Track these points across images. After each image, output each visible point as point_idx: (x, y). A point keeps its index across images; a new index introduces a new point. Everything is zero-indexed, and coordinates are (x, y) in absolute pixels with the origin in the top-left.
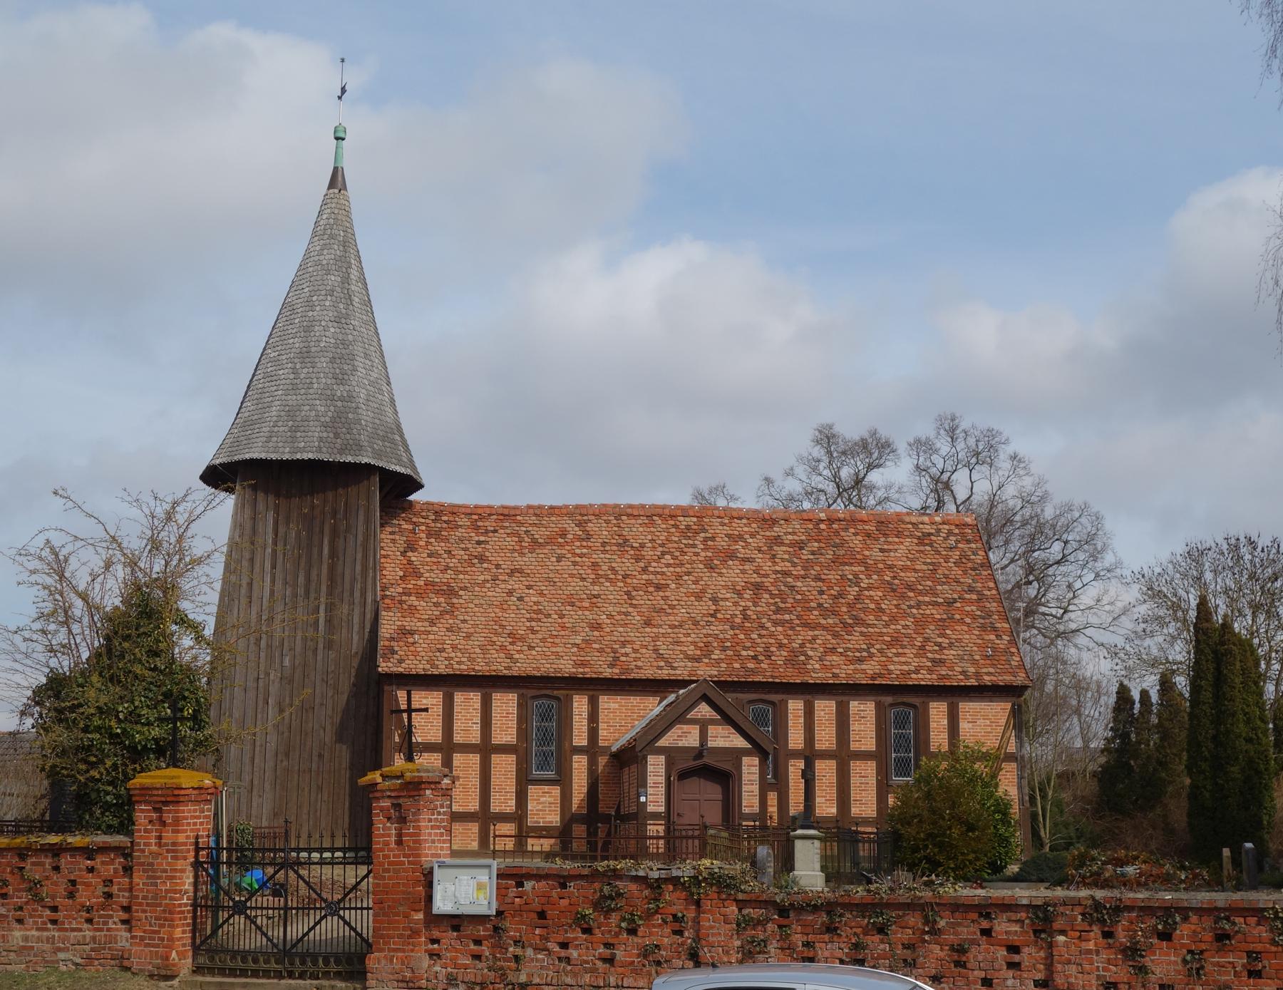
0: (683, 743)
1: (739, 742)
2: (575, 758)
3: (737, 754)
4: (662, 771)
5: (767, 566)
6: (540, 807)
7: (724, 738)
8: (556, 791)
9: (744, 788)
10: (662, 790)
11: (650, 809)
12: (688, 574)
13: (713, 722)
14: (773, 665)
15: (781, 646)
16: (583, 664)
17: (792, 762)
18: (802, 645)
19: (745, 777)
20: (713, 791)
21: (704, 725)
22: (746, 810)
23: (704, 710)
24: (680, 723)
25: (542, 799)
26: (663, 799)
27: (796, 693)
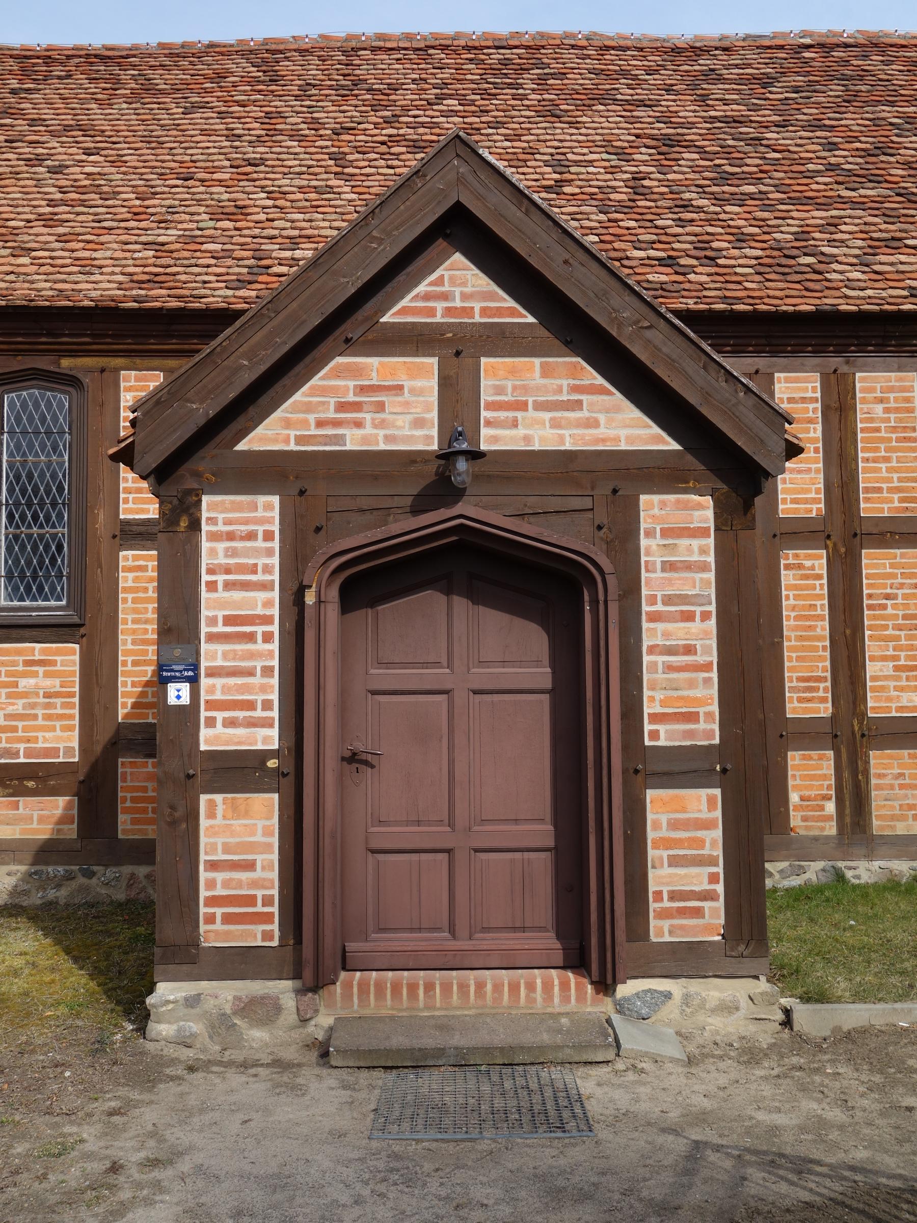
0: (360, 437)
1: (624, 427)
2: (127, 557)
3: (617, 480)
4: (269, 561)
5: (688, 111)
6: (18, 707)
7: (553, 410)
8: (68, 657)
9: (652, 634)
10: (269, 652)
11: (213, 737)
12: (497, 124)
13: (500, 340)
14: (727, 277)
15: (741, 239)
16: (154, 281)
17: (789, 557)
18: (802, 235)
19: (653, 584)
20: (509, 651)
21: (458, 350)
22: (661, 735)
23: (458, 288)
24: (350, 346)
25: (25, 683)
26: (269, 690)
27: (797, 351)
